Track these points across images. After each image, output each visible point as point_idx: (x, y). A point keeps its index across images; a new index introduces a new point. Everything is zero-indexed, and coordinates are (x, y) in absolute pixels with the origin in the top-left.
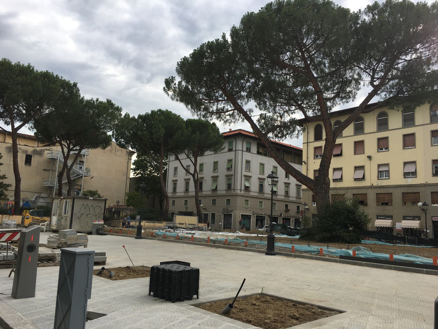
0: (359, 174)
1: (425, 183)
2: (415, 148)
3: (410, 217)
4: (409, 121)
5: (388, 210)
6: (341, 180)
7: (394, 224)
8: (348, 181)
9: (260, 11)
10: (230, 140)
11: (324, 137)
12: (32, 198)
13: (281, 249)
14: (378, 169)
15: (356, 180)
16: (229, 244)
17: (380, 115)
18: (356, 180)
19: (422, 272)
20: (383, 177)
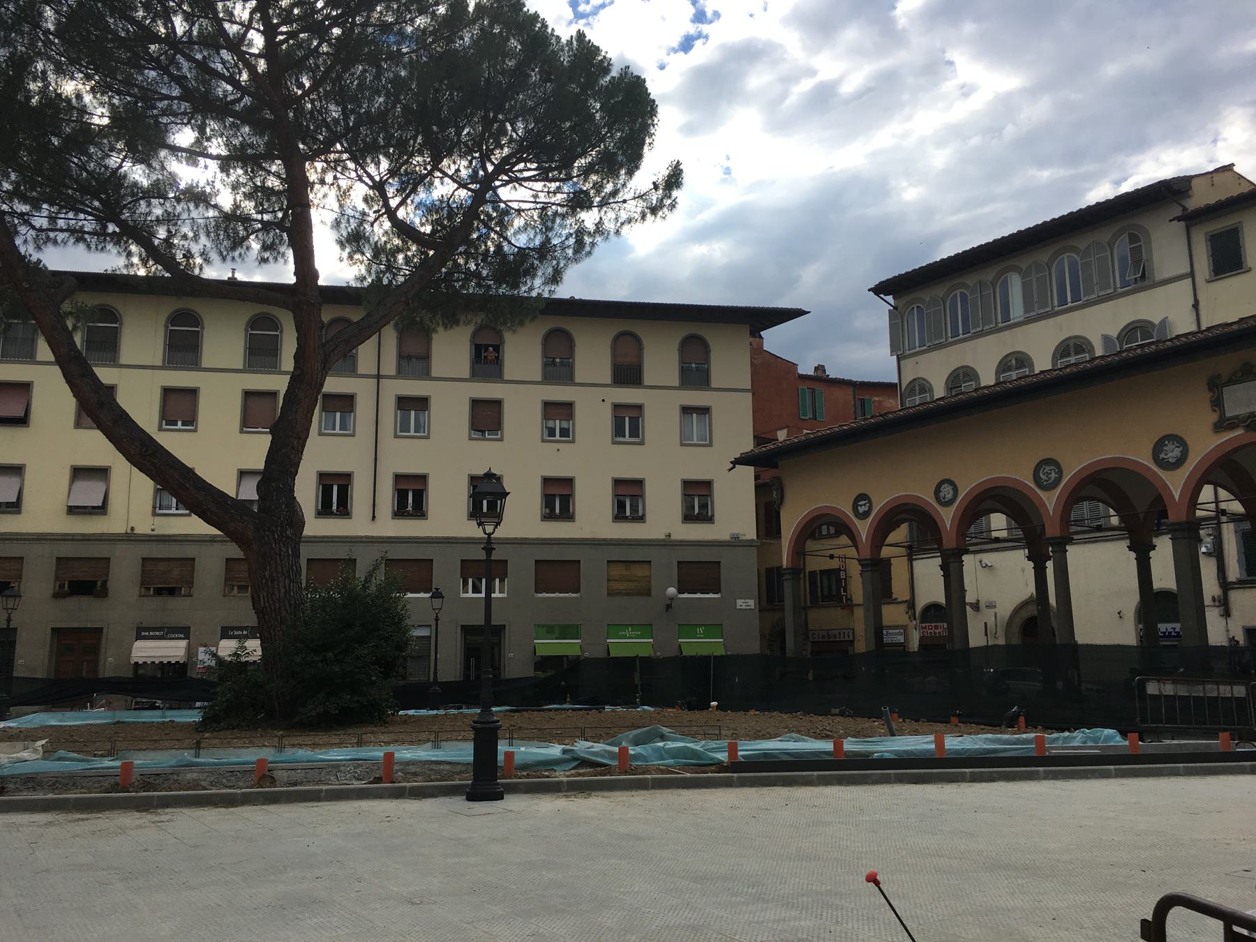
0: (89, 493)
2: (195, 431)
3: (241, 629)
4: (486, 360)
5: (176, 609)
6: (102, 509)
7: (191, 652)
8: (371, 520)
11: (288, 363)
13: (412, 769)
15: (72, 510)
16: (147, 786)
17: (175, 319)
18: (72, 510)
19: (1176, 773)
20: (170, 508)
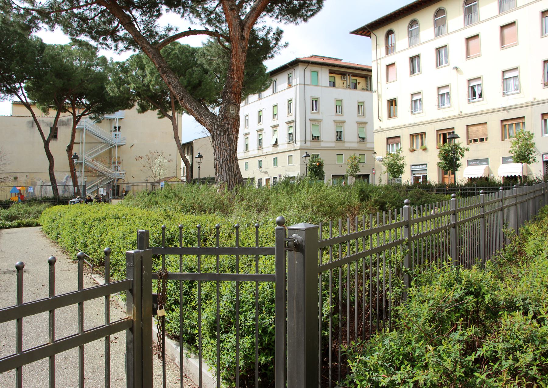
1: (532, 100)
9: (143, 109)
10: (289, 72)
12: (62, 179)
14: (503, 76)
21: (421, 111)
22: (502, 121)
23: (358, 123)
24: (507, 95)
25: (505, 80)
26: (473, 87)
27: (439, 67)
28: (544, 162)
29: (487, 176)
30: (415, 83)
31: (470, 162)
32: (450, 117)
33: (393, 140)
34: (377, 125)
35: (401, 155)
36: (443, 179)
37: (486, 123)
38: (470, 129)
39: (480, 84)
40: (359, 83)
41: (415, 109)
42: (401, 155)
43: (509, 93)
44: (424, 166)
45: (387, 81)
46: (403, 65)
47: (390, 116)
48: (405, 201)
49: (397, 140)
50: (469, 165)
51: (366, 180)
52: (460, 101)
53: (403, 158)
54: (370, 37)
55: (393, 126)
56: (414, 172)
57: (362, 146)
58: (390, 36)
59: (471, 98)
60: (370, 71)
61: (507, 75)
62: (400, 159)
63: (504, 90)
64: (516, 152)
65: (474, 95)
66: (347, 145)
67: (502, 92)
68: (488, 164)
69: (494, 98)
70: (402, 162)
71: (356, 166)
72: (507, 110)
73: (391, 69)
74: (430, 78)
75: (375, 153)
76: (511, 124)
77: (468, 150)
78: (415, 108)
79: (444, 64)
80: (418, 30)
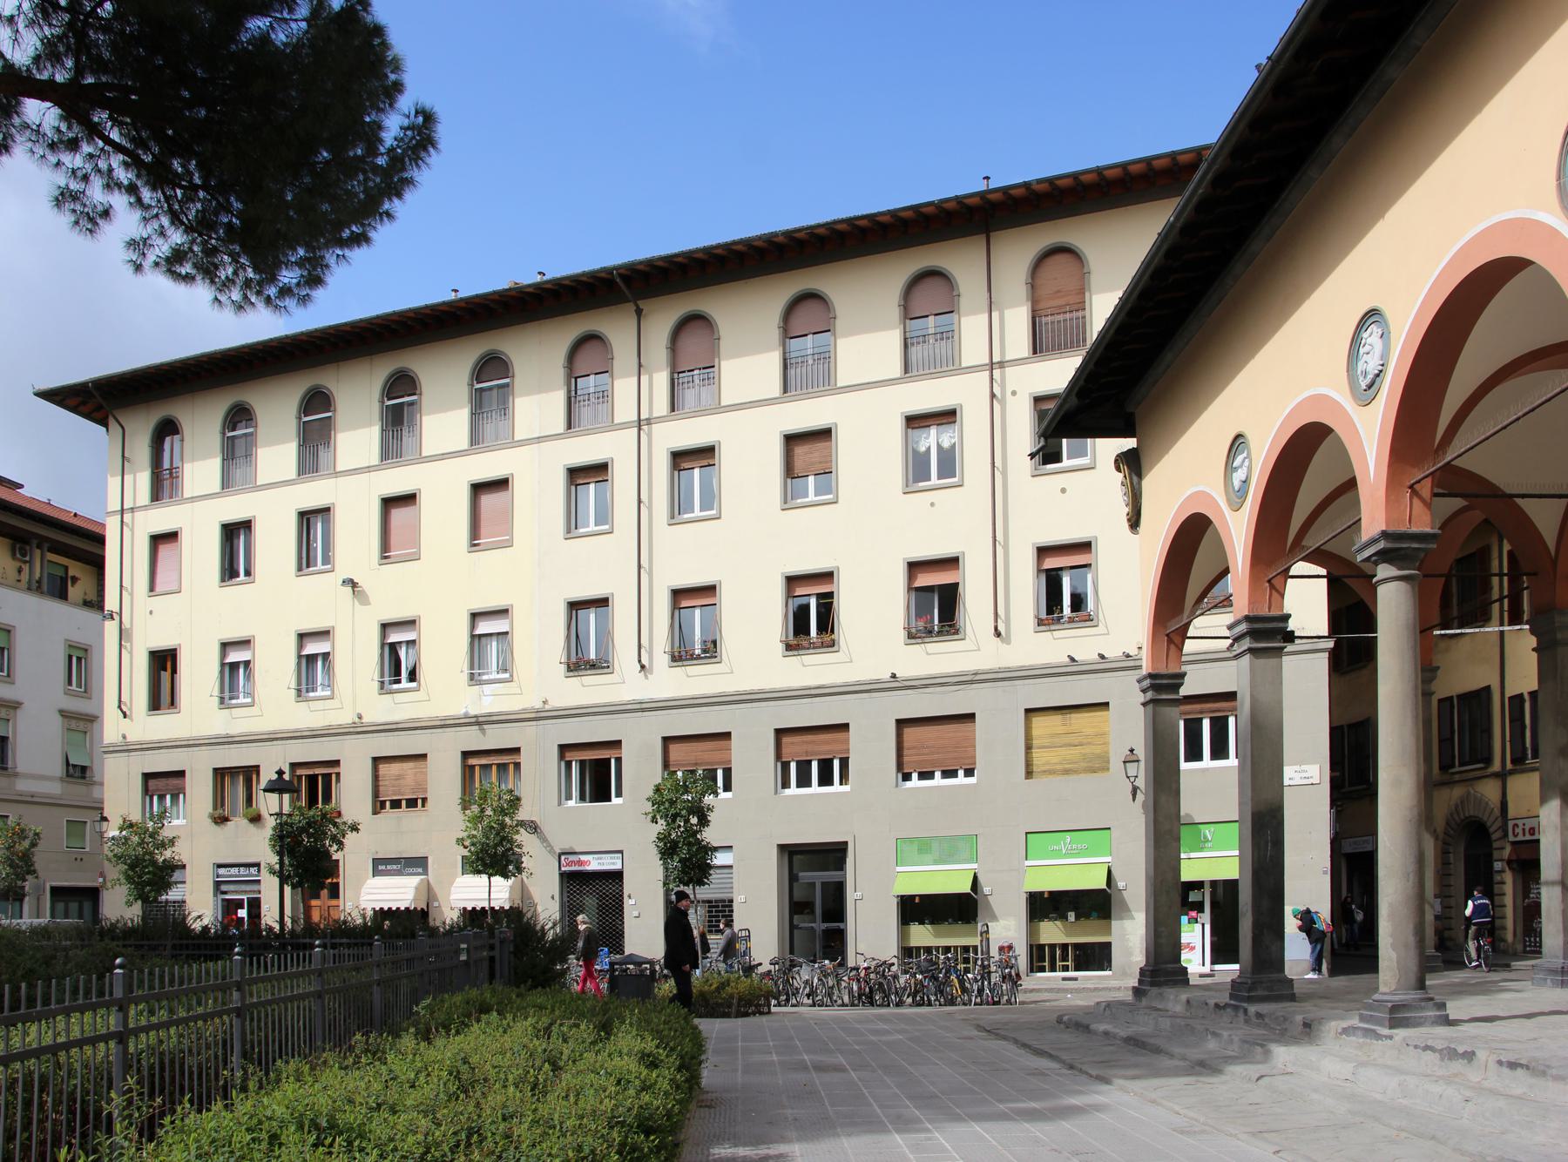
1: (538, 705)
14: (473, 627)
21: (249, 700)
22: (466, 755)
23: (64, 714)
24: (481, 683)
25: (476, 639)
26: (393, 647)
27: (306, 571)
28: (563, 875)
29: (422, 905)
30: (234, 612)
31: (381, 866)
32: (329, 727)
33: (162, 784)
34: (113, 728)
35: (166, 833)
36: (308, 910)
37: (424, 756)
38: (384, 769)
39: (413, 642)
40: (75, 580)
41: (232, 690)
42: (166, 833)
43: (485, 677)
44: (253, 870)
45: (152, 588)
46: (201, 550)
47: (155, 704)
48: (118, 961)
49: (174, 781)
50: (376, 873)
51: (87, 906)
52: (356, 688)
53: (172, 842)
54: (106, 425)
55: (164, 737)
56: (224, 888)
57: (77, 791)
58: (168, 440)
59: (387, 679)
60: (100, 540)
61: (484, 627)
62: (163, 845)
63: (472, 667)
64: (473, 844)
65: (397, 672)
66: (23, 786)
67: (467, 671)
68: (425, 872)
69: (444, 688)
70: (168, 854)
71: (26, 857)
72: (478, 723)
73: (164, 550)
74: (276, 603)
75: (105, 819)
76: (487, 769)
77: (357, 830)
78: (233, 688)
79: (320, 566)
80: (251, 440)
